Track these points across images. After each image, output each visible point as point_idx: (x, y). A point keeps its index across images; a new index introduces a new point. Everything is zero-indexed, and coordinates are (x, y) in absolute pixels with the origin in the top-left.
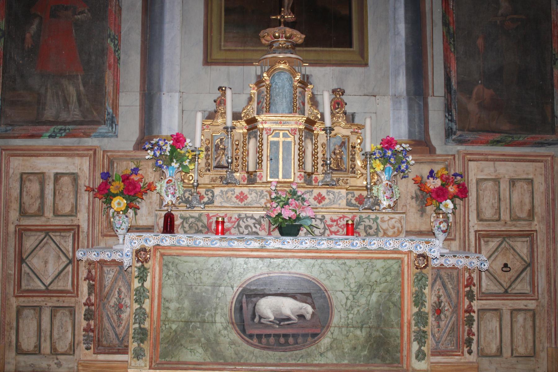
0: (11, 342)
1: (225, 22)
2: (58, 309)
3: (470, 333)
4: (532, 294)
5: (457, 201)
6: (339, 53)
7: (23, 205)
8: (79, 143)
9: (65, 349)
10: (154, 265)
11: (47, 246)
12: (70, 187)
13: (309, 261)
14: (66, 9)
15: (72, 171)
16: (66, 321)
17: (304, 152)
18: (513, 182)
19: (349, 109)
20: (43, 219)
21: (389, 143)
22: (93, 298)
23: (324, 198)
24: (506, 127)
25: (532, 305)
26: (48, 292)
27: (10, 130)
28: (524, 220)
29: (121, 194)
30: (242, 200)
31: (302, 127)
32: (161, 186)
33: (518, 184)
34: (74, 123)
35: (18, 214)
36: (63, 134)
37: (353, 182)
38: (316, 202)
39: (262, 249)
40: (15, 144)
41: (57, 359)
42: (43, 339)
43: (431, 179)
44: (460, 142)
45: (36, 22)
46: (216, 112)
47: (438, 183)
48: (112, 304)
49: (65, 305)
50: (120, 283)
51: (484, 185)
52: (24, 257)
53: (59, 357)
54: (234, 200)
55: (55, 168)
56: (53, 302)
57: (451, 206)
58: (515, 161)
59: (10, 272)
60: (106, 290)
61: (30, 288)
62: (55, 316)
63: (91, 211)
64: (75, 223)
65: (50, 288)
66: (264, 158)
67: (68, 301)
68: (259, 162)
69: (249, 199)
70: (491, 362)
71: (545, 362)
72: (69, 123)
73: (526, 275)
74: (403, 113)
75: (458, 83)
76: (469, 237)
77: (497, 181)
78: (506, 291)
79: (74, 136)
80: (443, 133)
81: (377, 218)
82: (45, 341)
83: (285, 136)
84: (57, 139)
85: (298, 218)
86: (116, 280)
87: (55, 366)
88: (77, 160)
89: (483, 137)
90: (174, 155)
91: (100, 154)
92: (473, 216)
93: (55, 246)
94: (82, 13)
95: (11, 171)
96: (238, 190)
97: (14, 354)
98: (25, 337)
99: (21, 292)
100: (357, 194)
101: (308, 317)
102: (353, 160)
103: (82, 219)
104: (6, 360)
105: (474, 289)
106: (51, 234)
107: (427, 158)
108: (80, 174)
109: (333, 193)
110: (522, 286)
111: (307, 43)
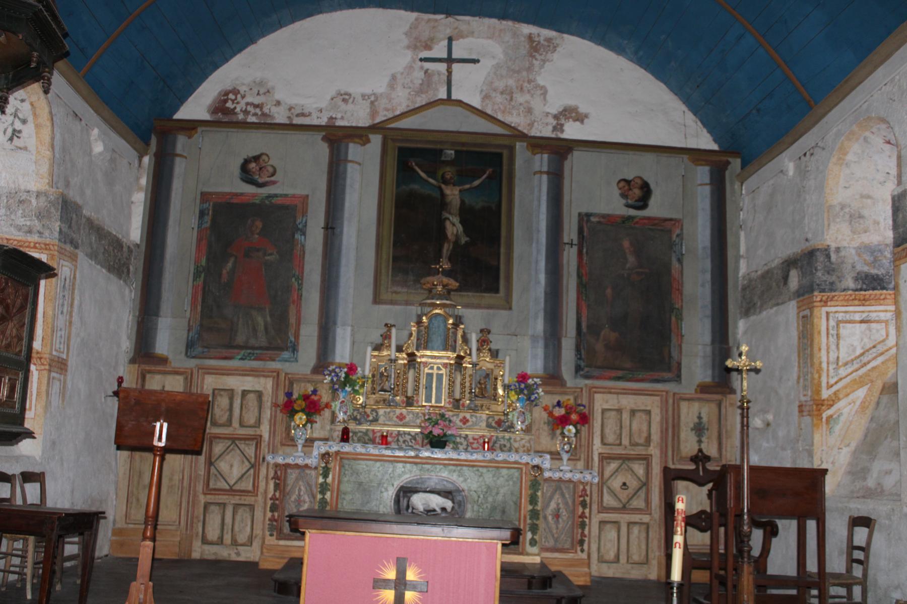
1: (393, 268)
3: (583, 535)
4: (647, 510)
5: (579, 426)
6: (488, 298)
10: (335, 466)
11: (233, 452)
12: (256, 403)
13: (451, 467)
14: (258, 250)
15: (257, 389)
17: (453, 382)
18: (633, 412)
19: (493, 346)
20: (231, 429)
21: (523, 378)
22: (277, 494)
23: (468, 421)
24: (628, 365)
25: (646, 519)
26: (231, 491)
28: (642, 445)
29: (303, 411)
30: (401, 420)
31: (452, 362)
32: (336, 405)
33: (638, 415)
34: (261, 348)
37: (494, 407)
38: (461, 424)
39: (417, 457)
42: (225, 532)
43: (557, 408)
44: (587, 377)
45: (232, 260)
46: (382, 345)
47: (562, 411)
48: (293, 499)
49: (246, 503)
50: (301, 483)
51: (607, 414)
53: (239, 548)
54: (395, 419)
56: (236, 500)
57: (574, 430)
58: (634, 394)
60: (289, 488)
61: (216, 487)
63: (273, 423)
64: (258, 433)
65: (234, 488)
66: (421, 386)
67: (249, 500)
68: (416, 389)
69: (407, 419)
70: (609, 568)
71: (656, 569)
72: (257, 348)
73: (642, 494)
74: (540, 352)
75: (588, 327)
77: (619, 411)
78: (624, 507)
79: (261, 360)
80: (573, 369)
81: (510, 438)
83: (438, 368)
84: (246, 361)
85: (445, 435)
86: (297, 479)
88: (262, 380)
89: (608, 373)
90: (348, 381)
91: (282, 376)
92: (597, 441)
94: (271, 254)
96: (398, 411)
97: (200, 543)
99: (208, 490)
100: (497, 418)
101: (449, 510)
102: (495, 389)
103: (265, 430)
104: (193, 549)
105: (588, 499)
106: (237, 442)
107: (558, 389)
109: (476, 417)
110: (639, 503)
111: (459, 290)
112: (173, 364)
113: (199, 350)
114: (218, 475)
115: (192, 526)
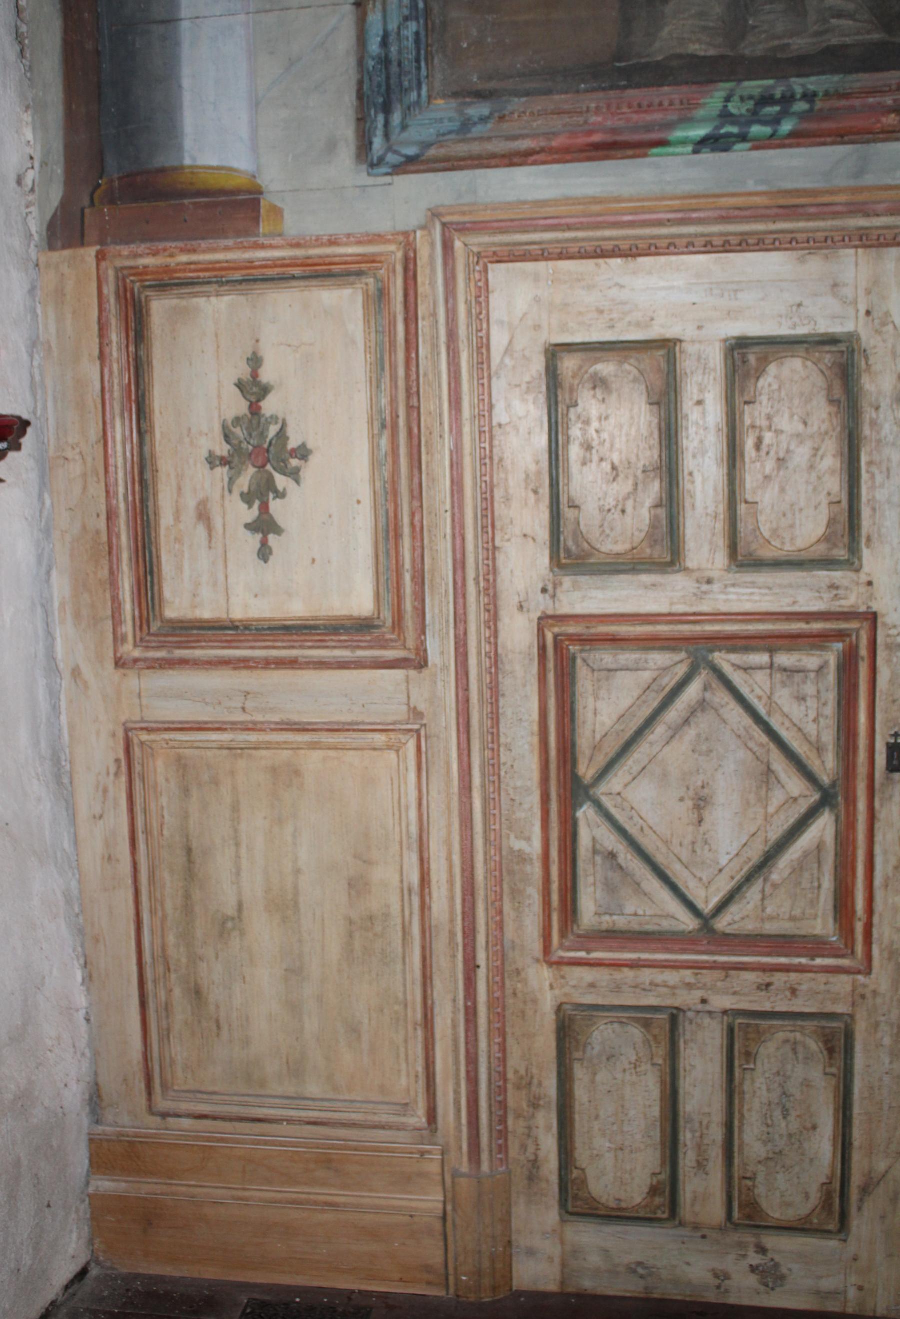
0: (535, 1163)
2: (765, 1024)
7: (568, 514)
8: (860, 173)
9: (804, 1210)
11: (704, 722)
15: (825, 327)
16: (807, 1084)
27: (484, 120)
35: (544, 560)
36: (787, 127)
40: (512, 196)
41: (762, 1250)
42: (688, 1159)
52: (586, 770)
53: (771, 1241)
55: (731, 314)
59: (518, 845)
61: (621, 922)
62: (749, 1056)
64: (852, 600)
76: (127, 489)
82: (701, 1165)
84: (741, 154)
87: (753, 1280)
93: (748, 721)
95: (499, 339)
97: (552, 1216)
98: (602, 1144)
106: (724, 660)
108: (867, 338)
112: (293, 224)
113: (432, 118)
114: (627, 857)
115: (502, 1134)
